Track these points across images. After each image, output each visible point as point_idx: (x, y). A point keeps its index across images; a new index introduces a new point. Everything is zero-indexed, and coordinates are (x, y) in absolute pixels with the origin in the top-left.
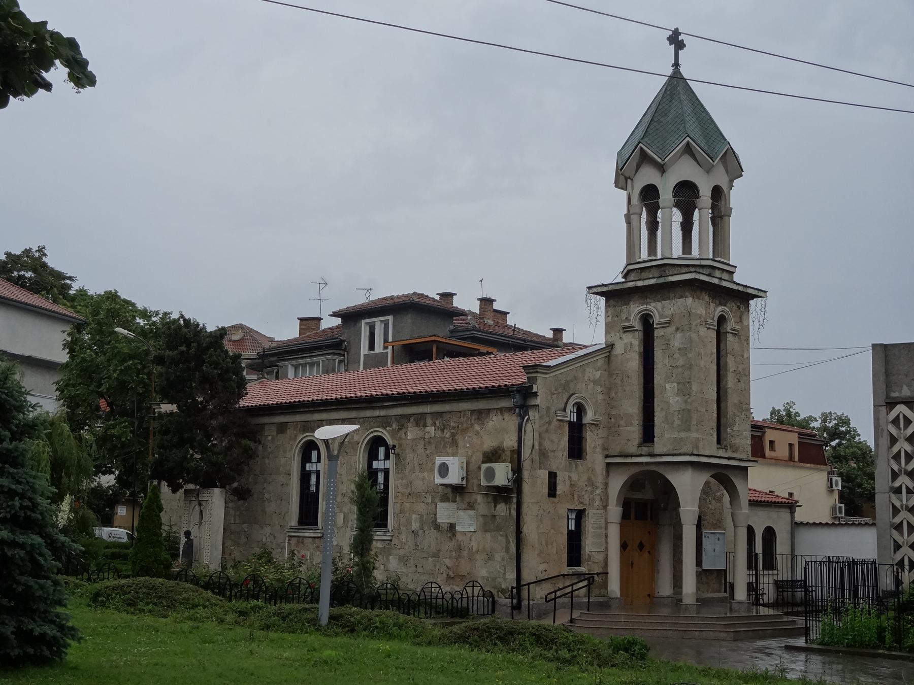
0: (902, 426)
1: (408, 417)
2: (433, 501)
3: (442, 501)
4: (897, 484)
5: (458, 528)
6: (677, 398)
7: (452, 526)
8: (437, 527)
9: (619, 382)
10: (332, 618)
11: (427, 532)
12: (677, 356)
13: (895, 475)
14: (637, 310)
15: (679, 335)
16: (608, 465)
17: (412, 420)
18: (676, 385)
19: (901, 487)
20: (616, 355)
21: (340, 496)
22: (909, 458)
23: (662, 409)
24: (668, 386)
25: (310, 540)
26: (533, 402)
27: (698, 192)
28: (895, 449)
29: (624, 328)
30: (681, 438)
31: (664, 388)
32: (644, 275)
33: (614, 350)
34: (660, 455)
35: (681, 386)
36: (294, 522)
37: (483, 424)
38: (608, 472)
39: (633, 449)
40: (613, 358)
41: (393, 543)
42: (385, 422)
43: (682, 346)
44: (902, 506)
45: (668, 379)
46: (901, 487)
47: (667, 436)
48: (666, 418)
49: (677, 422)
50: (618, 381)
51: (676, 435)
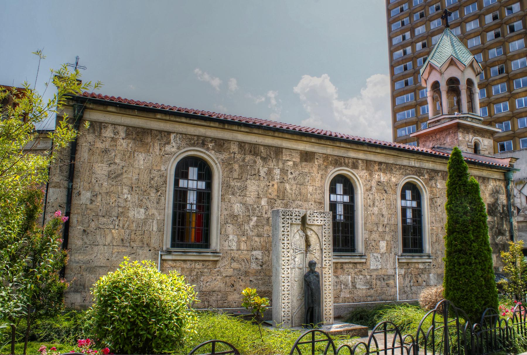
1: (436, 172)
17: (440, 174)
21: (381, 226)
25: (351, 266)
32: (474, 121)
36: (169, 246)
37: (486, 186)
41: (432, 264)
42: (419, 172)
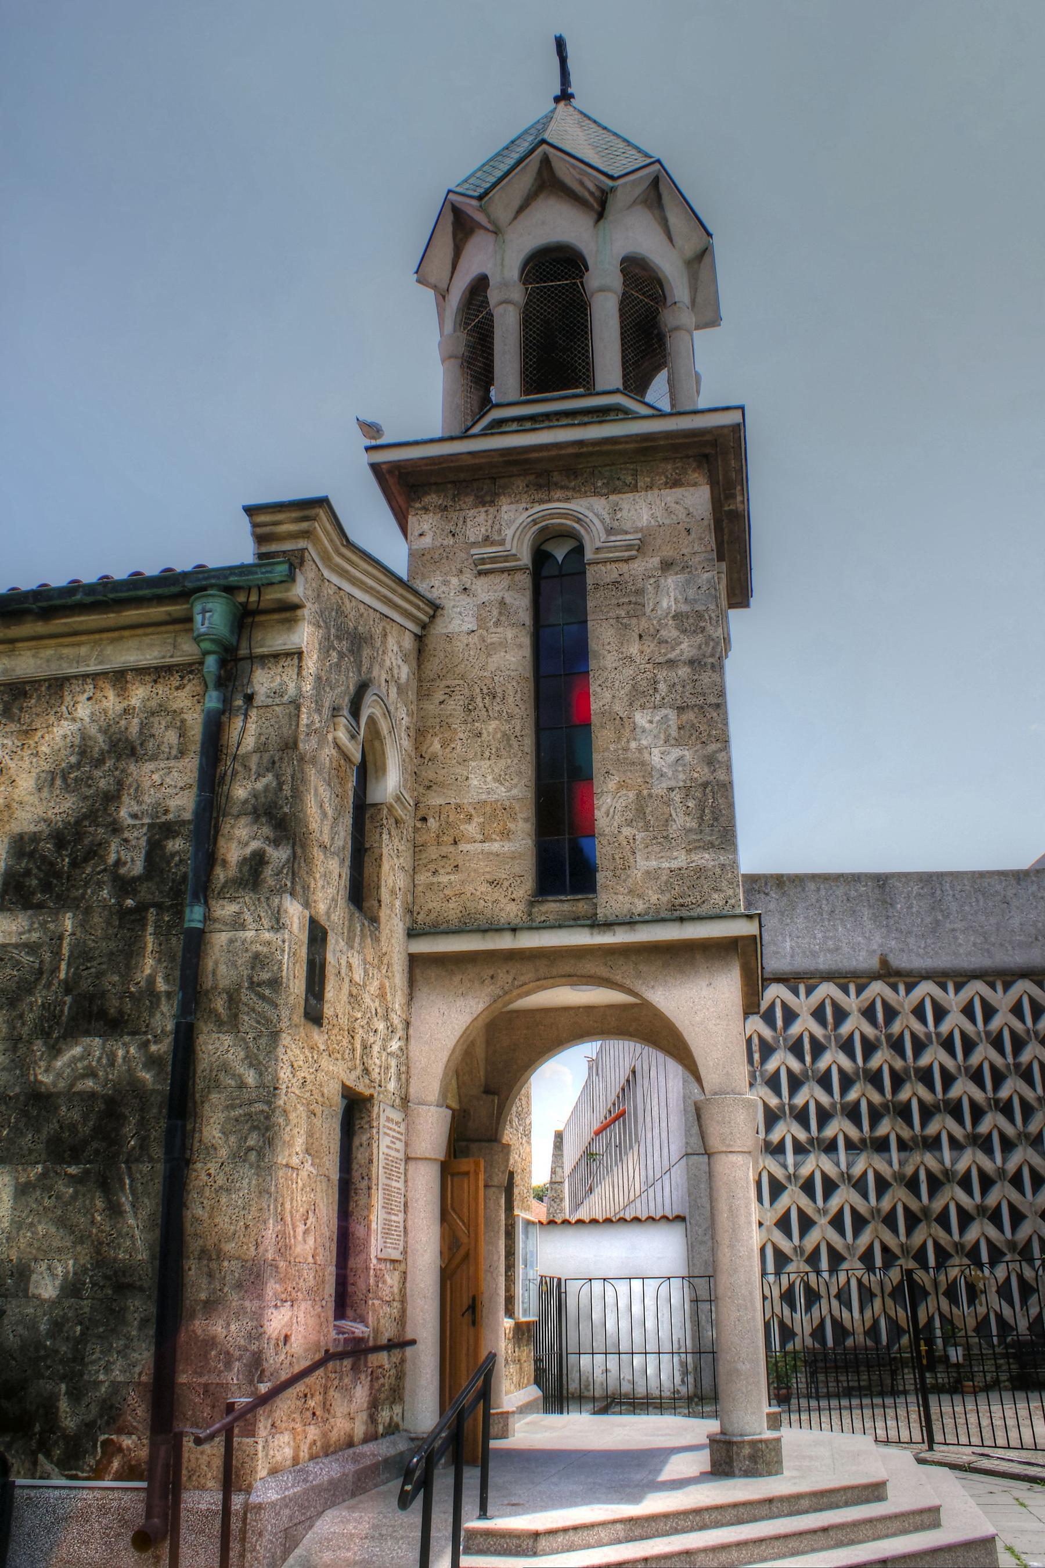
0: (780, 1023)
4: (775, 1137)
6: (676, 753)
9: (459, 712)
10: (680, 728)
12: (670, 632)
13: (771, 1118)
14: (523, 517)
15: (672, 582)
16: (414, 961)
18: (672, 715)
19: (783, 1141)
20: (449, 638)
22: (1038, 1011)
23: (622, 785)
24: (641, 719)
26: (278, 641)
27: (621, 302)
28: (771, 1066)
29: (483, 561)
30: (700, 870)
31: (622, 723)
33: (439, 621)
34: (630, 922)
35: (690, 716)
38: (412, 982)
39: (512, 911)
40: (432, 642)
43: (685, 608)
44: (789, 1177)
45: (641, 694)
46: (783, 1141)
47: (643, 864)
48: (641, 811)
49: (681, 821)
50: (455, 706)
51: (680, 859)
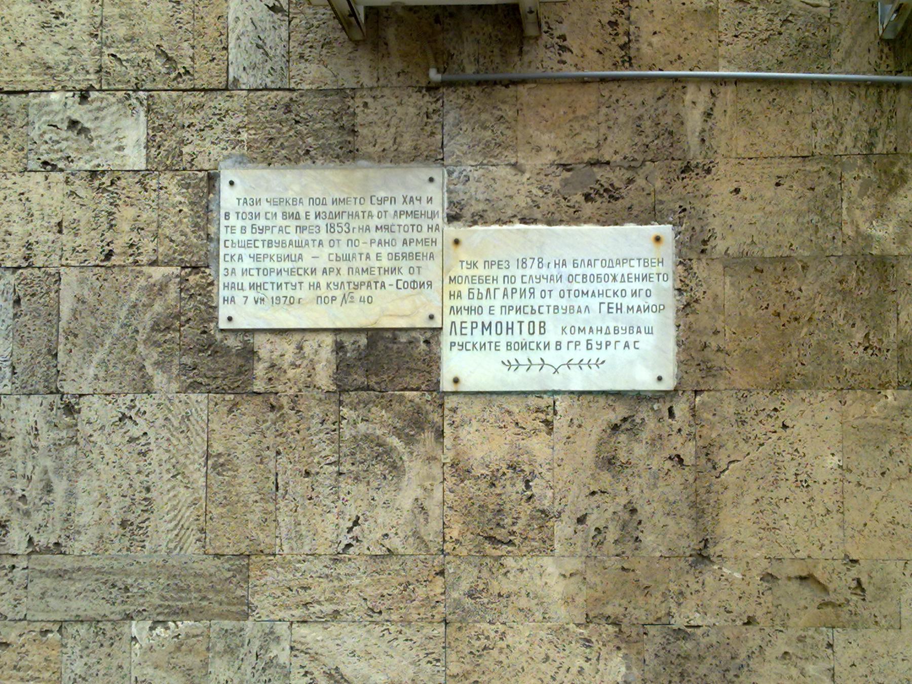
2: (165, 156)
3: (268, 153)
5: (466, 366)
7: (386, 365)
8: (225, 364)
11: (96, 410)
